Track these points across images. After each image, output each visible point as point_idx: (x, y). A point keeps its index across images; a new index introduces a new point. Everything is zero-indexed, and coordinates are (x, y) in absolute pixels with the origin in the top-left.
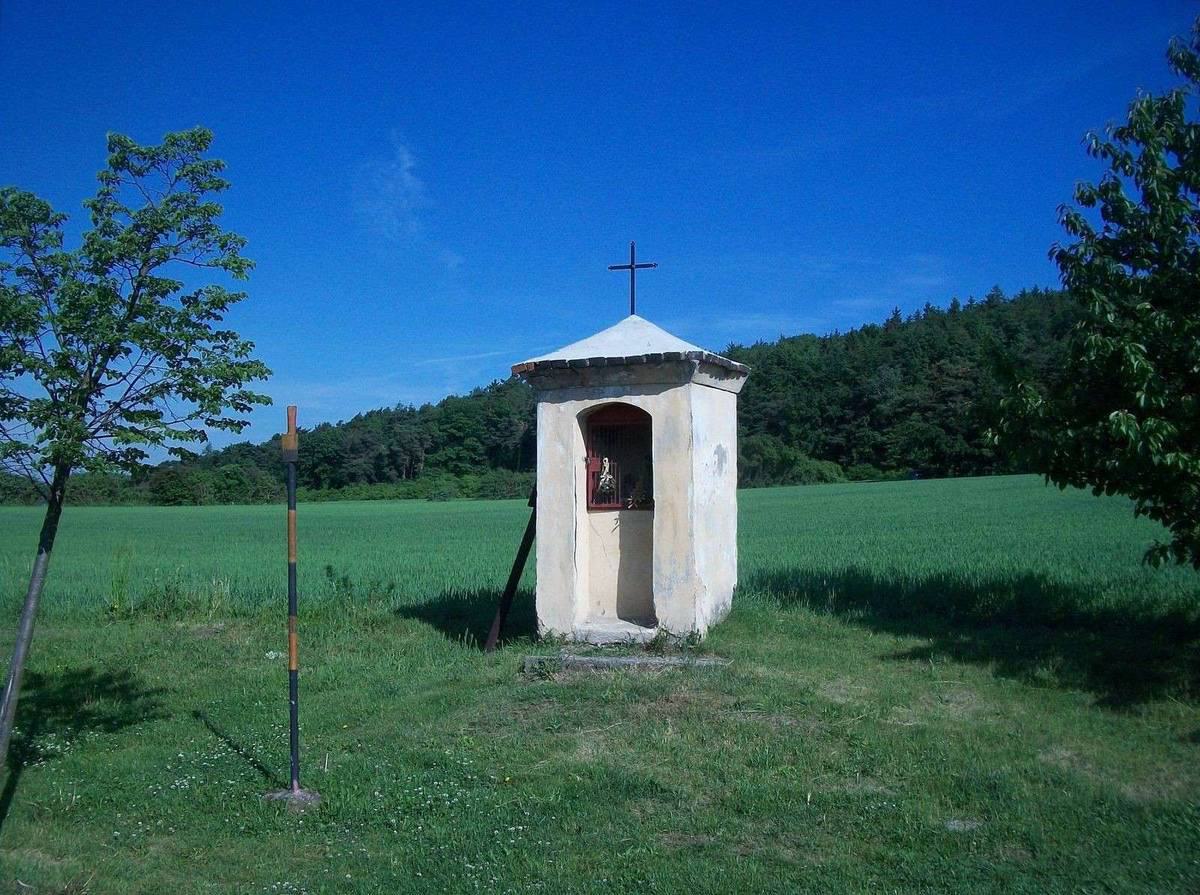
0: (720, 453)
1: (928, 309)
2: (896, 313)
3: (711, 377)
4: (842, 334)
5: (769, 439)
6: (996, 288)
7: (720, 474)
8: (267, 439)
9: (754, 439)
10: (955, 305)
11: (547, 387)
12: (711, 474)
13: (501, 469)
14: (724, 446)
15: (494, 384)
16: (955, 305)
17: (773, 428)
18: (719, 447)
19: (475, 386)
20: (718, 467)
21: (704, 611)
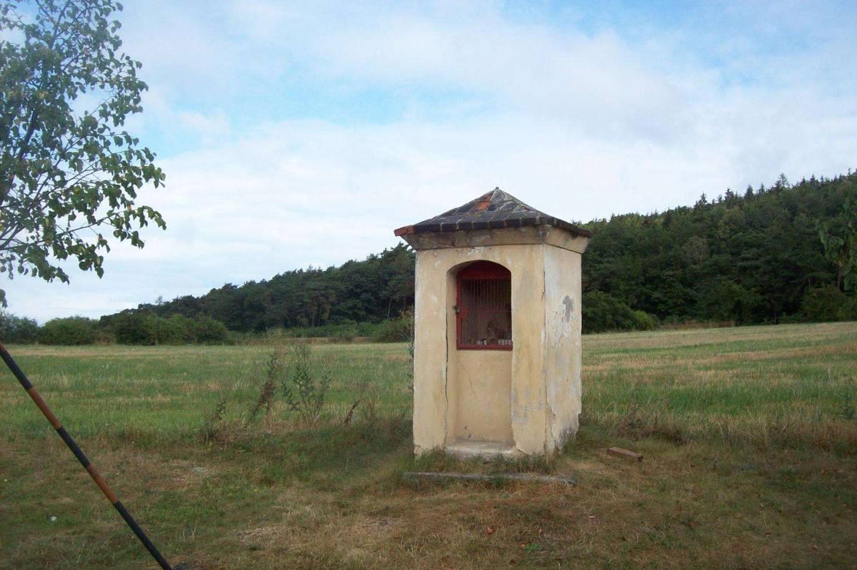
0: (568, 302)
1: (729, 193)
2: (703, 197)
3: (301, 270)
4: (660, 213)
5: (602, 295)
6: (783, 176)
7: (568, 321)
8: (396, 246)
9: (592, 295)
10: (750, 190)
11: (424, 247)
12: (560, 321)
13: (565, 305)
14: (571, 297)
15: (385, 251)
16: (750, 190)
17: (606, 287)
18: (567, 298)
19: (350, 259)
20: (566, 315)
21: (554, 434)
